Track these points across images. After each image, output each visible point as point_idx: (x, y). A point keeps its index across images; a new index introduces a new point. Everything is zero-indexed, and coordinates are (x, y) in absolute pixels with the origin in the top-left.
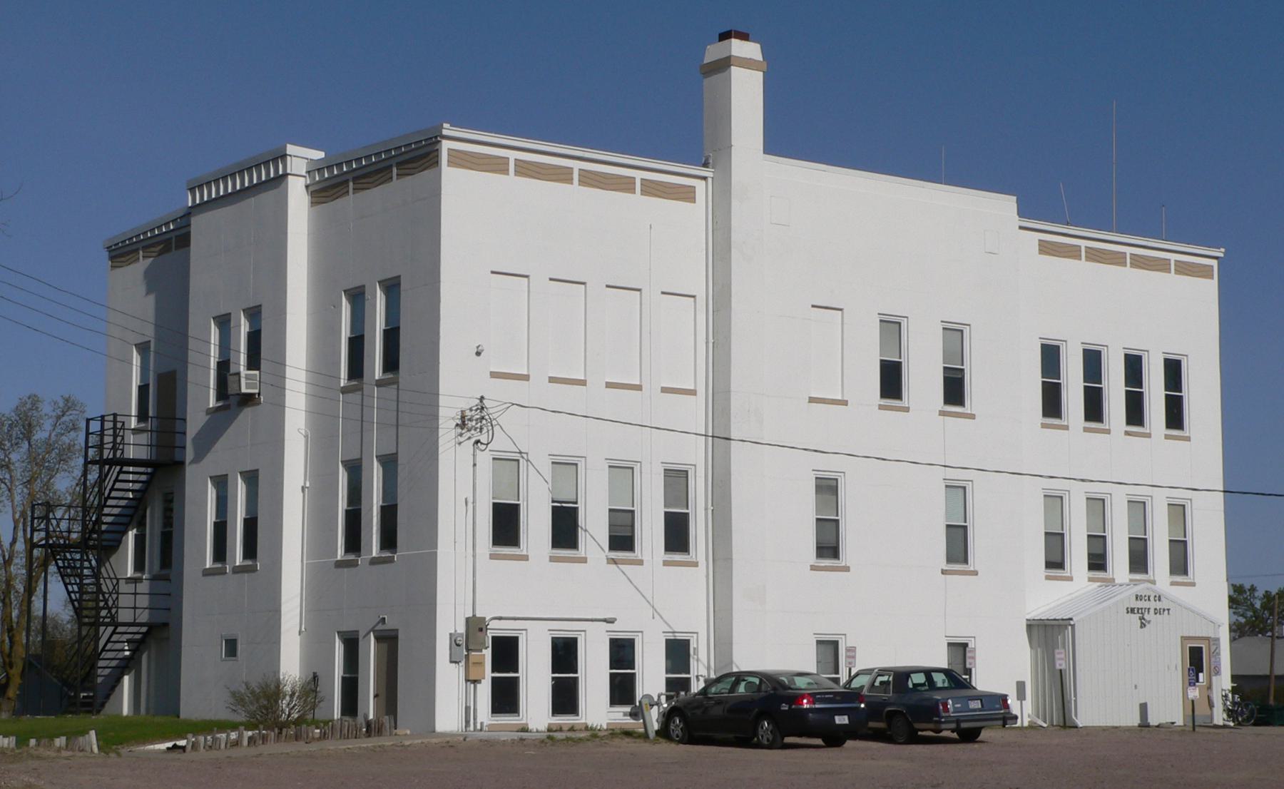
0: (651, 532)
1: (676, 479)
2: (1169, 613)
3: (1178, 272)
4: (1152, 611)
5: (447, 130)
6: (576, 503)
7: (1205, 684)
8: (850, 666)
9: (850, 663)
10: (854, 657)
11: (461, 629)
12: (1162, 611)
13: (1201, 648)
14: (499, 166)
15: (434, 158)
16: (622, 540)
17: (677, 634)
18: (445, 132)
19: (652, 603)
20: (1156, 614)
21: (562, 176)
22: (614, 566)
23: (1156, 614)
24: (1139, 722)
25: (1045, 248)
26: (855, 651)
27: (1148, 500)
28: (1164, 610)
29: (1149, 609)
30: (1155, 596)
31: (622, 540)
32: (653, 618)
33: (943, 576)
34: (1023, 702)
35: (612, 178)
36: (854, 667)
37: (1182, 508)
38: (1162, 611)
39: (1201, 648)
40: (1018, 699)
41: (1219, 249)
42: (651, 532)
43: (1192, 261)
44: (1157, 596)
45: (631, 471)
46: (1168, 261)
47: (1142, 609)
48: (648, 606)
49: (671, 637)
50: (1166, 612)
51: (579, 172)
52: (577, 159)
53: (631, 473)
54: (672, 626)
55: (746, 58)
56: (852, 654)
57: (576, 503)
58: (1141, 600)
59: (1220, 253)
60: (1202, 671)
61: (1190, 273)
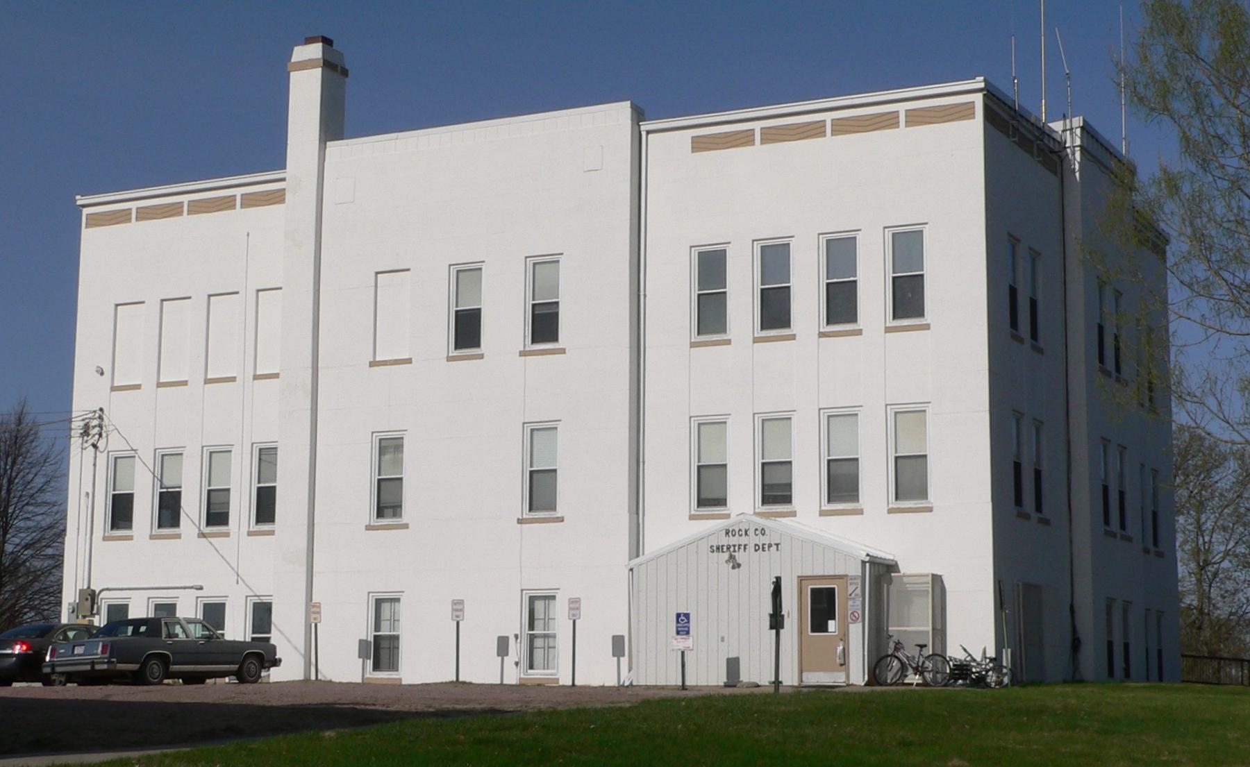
0: (242, 507)
1: (266, 457)
2: (777, 549)
3: (909, 123)
4: (751, 548)
5: (80, 201)
6: (180, 487)
7: (836, 633)
8: (458, 619)
9: (574, 615)
10: (578, 609)
11: (775, 580)
12: (766, 547)
13: (813, 590)
14: (816, 130)
15: (280, 196)
16: (217, 516)
17: (262, 598)
18: (79, 203)
19: (236, 569)
20: (756, 550)
21: (175, 210)
22: (204, 539)
23: (756, 550)
24: (725, 680)
25: (699, 145)
26: (319, 607)
27: (112, 455)
28: (770, 546)
29: (745, 545)
30: (756, 530)
31: (217, 516)
32: (238, 583)
33: (519, 525)
34: (505, 658)
35: (801, 127)
36: (320, 622)
37: (831, 419)
38: (766, 547)
39: (813, 590)
40: (498, 655)
41: (974, 79)
42: (242, 507)
43: (850, 115)
44: (760, 529)
45: (119, 460)
46: (896, 114)
47: (734, 546)
48: (233, 572)
49: (256, 600)
50: (775, 547)
51: (832, 122)
52: (756, 119)
53: (121, 460)
54: (253, 589)
55: (305, 61)
56: (576, 605)
57: (180, 487)
58: (734, 536)
59: (979, 83)
60: (833, 618)
61: (861, 129)
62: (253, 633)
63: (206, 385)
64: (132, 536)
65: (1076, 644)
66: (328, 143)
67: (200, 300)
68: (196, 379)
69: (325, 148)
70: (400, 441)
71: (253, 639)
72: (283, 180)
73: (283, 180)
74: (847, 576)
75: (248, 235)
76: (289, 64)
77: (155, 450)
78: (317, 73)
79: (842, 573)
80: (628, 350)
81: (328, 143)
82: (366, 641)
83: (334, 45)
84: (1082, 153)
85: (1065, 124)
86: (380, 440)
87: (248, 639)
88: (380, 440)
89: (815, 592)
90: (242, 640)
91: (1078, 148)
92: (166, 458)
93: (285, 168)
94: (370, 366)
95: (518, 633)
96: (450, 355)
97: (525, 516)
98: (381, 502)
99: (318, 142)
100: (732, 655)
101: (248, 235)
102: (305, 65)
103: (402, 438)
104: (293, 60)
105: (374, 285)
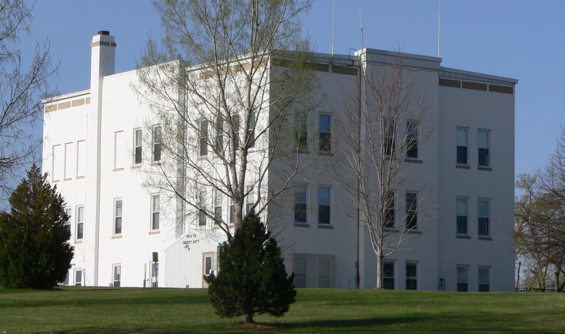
13: (207, 258)
39: (207, 258)
62: (76, 282)
63: (77, 180)
64: (122, 236)
65: (357, 266)
66: (104, 77)
67: (63, 146)
68: (74, 178)
69: (103, 79)
70: (121, 202)
71: (76, 284)
72: (89, 93)
73: (89, 93)
74: (214, 252)
75: (87, 115)
76: (91, 44)
77: (76, 206)
78: (99, 47)
79: (213, 251)
80: (96, 173)
81: (104, 77)
82: (112, 284)
83: (110, 34)
84: (367, 64)
85: (362, 51)
86: (117, 202)
87: (75, 285)
88: (117, 202)
89: (77, 272)
90: (72, 285)
91: (365, 62)
92: (81, 209)
93: (90, 88)
94: (114, 171)
95: (149, 279)
96: (134, 166)
97: (151, 231)
98: (118, 227)
99: (99, 77)
100: (187, 284)
101: (87, 115)
102: (95, 44)
103: (122, 201)
104: (92, 42)
105: (114, 137)
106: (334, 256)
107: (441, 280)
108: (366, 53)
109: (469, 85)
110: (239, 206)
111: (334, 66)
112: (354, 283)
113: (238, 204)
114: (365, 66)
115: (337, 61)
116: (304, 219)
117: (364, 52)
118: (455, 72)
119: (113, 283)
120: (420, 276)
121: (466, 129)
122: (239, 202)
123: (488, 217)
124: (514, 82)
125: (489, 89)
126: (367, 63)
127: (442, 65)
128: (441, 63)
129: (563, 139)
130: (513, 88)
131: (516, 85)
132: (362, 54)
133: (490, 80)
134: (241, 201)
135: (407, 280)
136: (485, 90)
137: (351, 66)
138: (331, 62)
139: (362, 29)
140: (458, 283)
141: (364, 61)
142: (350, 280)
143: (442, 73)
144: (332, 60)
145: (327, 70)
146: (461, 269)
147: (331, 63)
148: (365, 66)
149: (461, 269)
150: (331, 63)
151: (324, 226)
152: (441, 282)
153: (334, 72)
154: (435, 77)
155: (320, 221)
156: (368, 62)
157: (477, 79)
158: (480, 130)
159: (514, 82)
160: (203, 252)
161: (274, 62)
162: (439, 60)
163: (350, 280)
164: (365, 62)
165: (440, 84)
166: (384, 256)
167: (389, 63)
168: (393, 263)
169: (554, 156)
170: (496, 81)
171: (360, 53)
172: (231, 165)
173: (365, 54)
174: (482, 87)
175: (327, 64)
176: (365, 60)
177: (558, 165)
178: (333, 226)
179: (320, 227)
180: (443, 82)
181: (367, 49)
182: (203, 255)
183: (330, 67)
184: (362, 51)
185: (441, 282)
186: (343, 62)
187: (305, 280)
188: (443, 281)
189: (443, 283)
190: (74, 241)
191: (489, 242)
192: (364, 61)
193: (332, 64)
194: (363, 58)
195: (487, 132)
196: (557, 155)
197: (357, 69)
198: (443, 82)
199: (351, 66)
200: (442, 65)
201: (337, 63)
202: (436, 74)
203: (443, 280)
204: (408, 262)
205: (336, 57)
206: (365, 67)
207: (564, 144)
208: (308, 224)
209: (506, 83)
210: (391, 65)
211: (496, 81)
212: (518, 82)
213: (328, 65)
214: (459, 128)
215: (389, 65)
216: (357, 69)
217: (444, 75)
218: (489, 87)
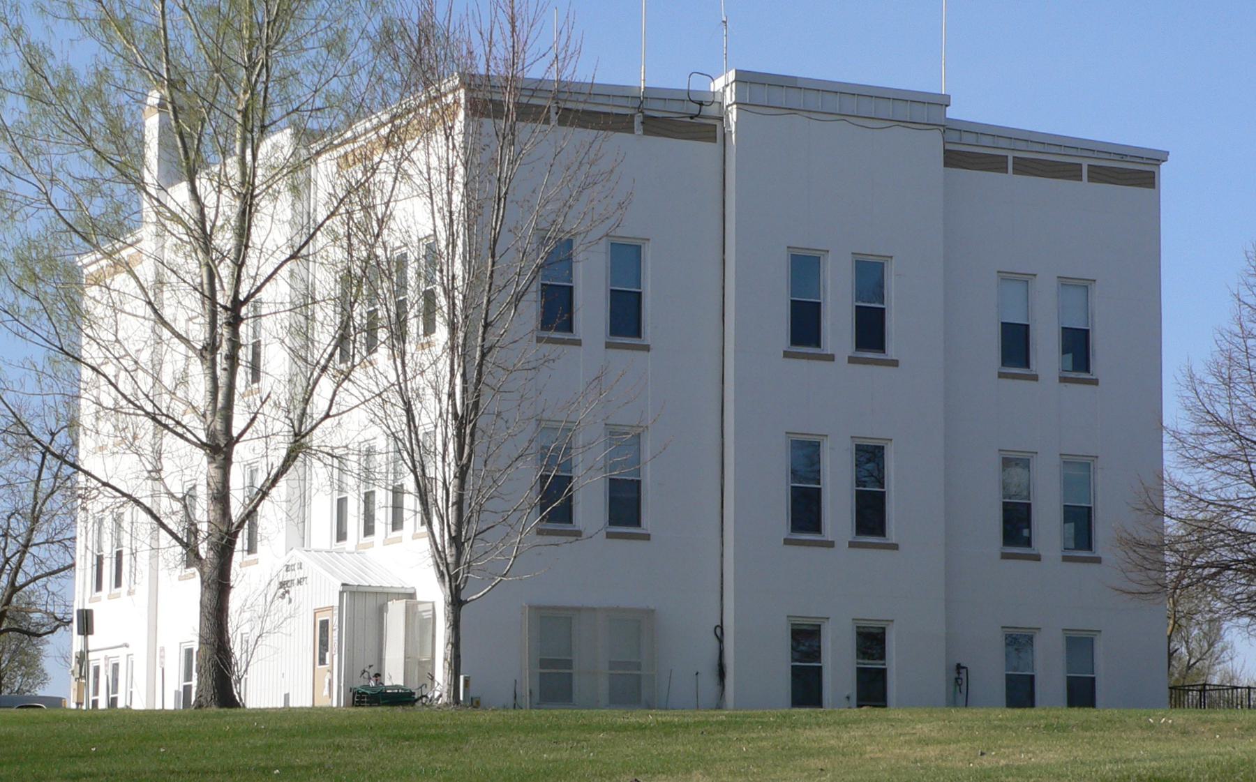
85: (727, 79)
106: (653, 611)
107: (959, 667)
108: (736, 81)
109: (1026, 167)
110: (216, 470)
111: (646, 117)
112: (710, 680)
113: (214, 465)
114: (733, 116)
115: (658, 105)
116: (564, 514)
117: (730, 80)
118: (834, 90)
119: (181, 690)
120: (894, 661)
121: (1025, 279)
122: (220, 458)
123: (1092, 505)
124: (1158, 158)
125: (1089, 177)
126: (737, 108)
127: (951, 113)
128: (948, 108)
129: (1250, 287)
130: (1156, 174)
131: (1163, 166)
132: (727, 86)
133: (1090, 154)
134: (223, 456)
135: (861, 672)
136: (1079, 177)
137: (697, 116)
138: (639, 108)
139: (725, 22)
140: (1007, 675)
141: (731, 105)
142: (697, 674)
143: (954, 136)
144: (642, 102)
145: (629, 129)
146: (1018, 642)
147: (640, 109)
148: (733, 116)
149: (1018, 642)
150: (640, 109)
151: (806, 540)
152: (959, 673)
153: (647, 132)
154: (933, 144)
155: (614, 519)
156: (741, 106)
157: (1073, 152)
158: (1065, 282)
159: (1158, 158)
160: (314, 608)
161: (476, 109)
162: (944, 102)
163: (697, 674)
164: (735, 106)
165: (946, 164)
166: (466, 602)
167: (802, 108)
168: (884, 629)
169: (1224, 333)
170: (1107, 156)
171: (723, 85)
172: (201, 355)
173: (734, 84)
174: (1069, 172)
175: (629, 112)
176: (734, 99)
177: (1242, 356)
178: (649, 532)
179: (1005, 556)
180: (953, 159)
181: (736, 71)
182: (315, 613)
183: (638, 119)
184: (727, 79)
185: (959, 673)
186: (676, 107)
187: (570, 675)
188: (964, 671)
189: (963, 676)
190: (128, 589)
191: (1094, 567)
192: (731, 105)
193: (641, 112)
194: (730, 97)
195: (1085, 285)
196: (1237, 329)
197: (716, 125)
198: (953, 159)
199: (697, 116)
200: (951, 113)
201: (656, 109)
202: (935, 138)
203: (964, 668)
204: (863, 624)
205: (650, 95)
206: (735, 120)
207: (1251, 300)
208: (576, 529)
209: (1132, 160)
210: (806, 114)
211: (1107, 156)
212: (1169, 157)
213: (632, 116)
214: (1006, 277)
215: (801, 113)
216: (716, 125)
217: (961, 139)
218: (1089, 171)
